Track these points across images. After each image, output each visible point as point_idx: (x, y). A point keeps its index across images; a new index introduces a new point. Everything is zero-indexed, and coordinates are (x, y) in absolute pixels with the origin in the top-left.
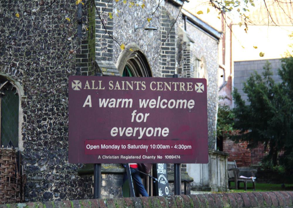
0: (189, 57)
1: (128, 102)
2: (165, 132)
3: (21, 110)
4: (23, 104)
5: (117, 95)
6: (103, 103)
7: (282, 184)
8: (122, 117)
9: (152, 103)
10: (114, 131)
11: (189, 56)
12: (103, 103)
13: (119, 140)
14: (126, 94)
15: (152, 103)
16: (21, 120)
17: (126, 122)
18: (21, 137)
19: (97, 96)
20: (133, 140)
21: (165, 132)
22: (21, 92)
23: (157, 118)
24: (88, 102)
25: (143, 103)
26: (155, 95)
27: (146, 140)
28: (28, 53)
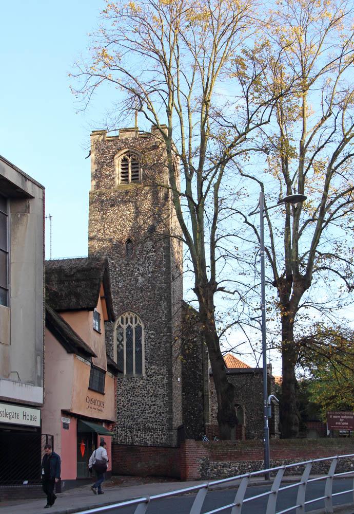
0: (122, 173)
1: (339, 417)
2: (347, 424)
3: (244, 414)
4: (245, 413)
5: (337, 415)
6: (334, 417)
7: (197, 169)
8: (338, 420)
9: (344, 417)
10: (336, 423)
11: (123, 171)
12: (334, 417)
13: (338, 425)
14: (339, 415)
15: (344, 417)
16: (245, 418)
17: (339, 421)
18: (245, 423)
19: (333, 415)
20: (341, 425)
21: (347, 424)
22: (244, 409)
23: (345, 420)
24: (331, 417)
25: (342, 417)
26: (345, 415)
27: (343, 425)
28: (247, 397)
